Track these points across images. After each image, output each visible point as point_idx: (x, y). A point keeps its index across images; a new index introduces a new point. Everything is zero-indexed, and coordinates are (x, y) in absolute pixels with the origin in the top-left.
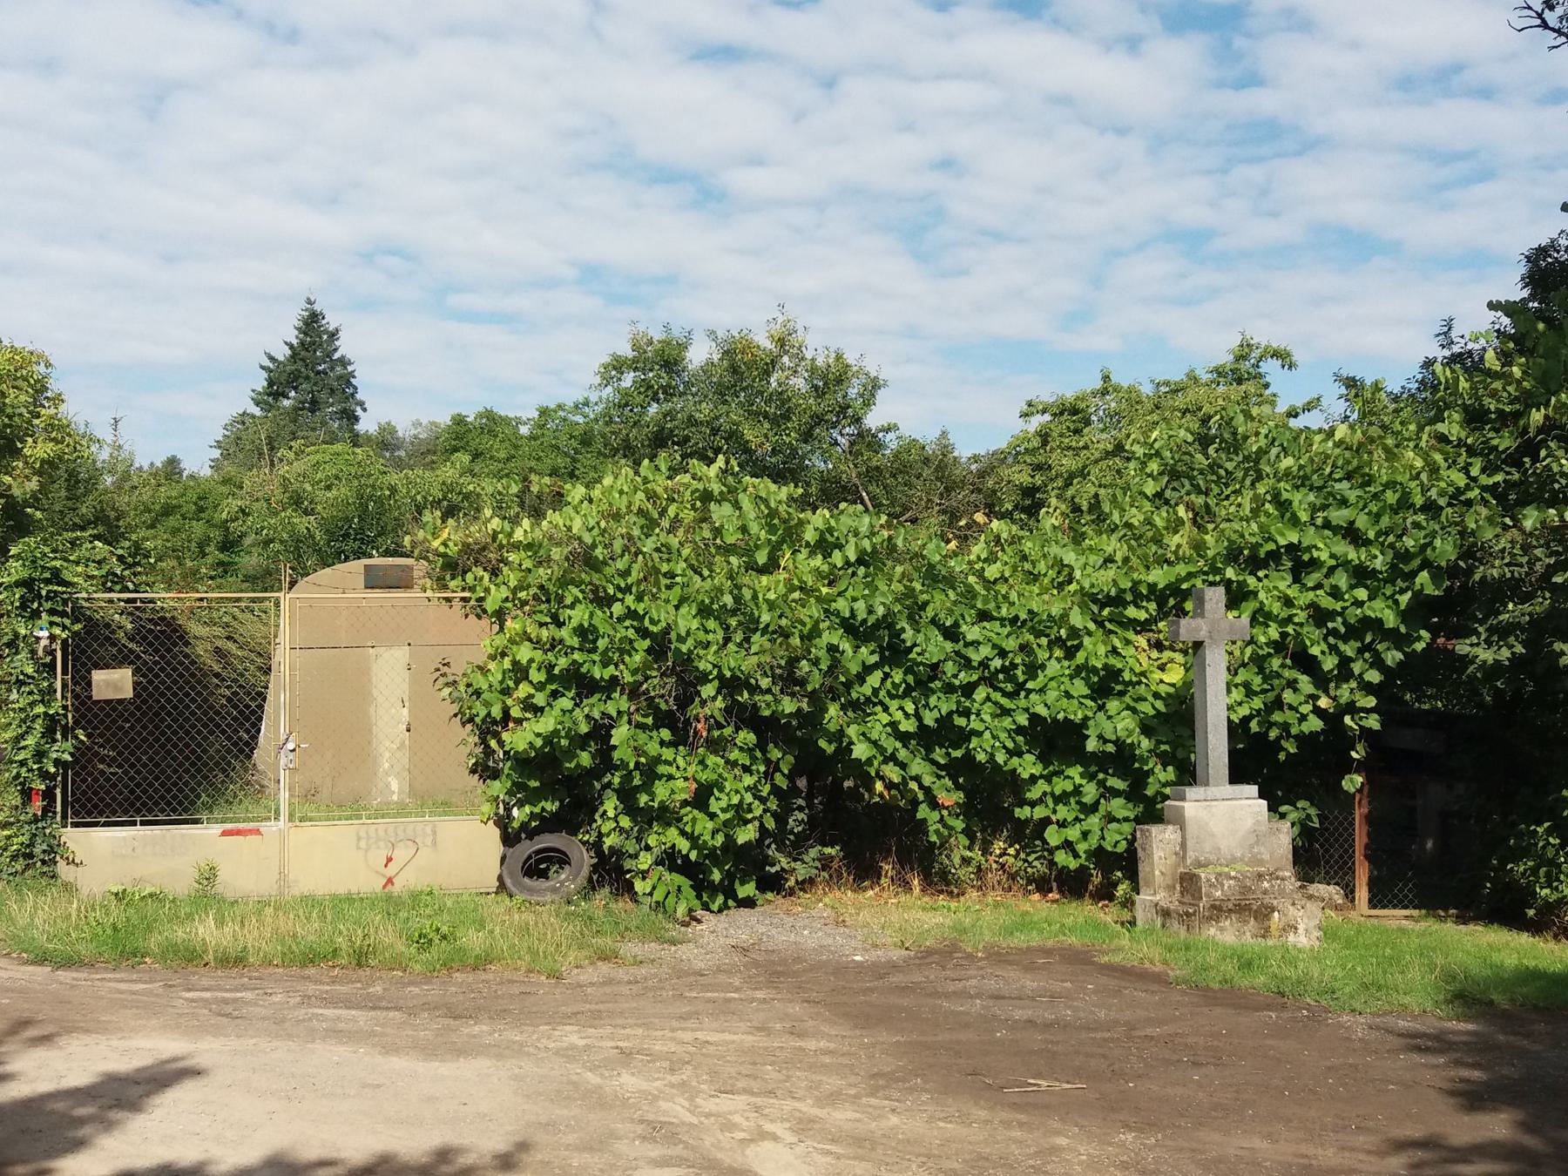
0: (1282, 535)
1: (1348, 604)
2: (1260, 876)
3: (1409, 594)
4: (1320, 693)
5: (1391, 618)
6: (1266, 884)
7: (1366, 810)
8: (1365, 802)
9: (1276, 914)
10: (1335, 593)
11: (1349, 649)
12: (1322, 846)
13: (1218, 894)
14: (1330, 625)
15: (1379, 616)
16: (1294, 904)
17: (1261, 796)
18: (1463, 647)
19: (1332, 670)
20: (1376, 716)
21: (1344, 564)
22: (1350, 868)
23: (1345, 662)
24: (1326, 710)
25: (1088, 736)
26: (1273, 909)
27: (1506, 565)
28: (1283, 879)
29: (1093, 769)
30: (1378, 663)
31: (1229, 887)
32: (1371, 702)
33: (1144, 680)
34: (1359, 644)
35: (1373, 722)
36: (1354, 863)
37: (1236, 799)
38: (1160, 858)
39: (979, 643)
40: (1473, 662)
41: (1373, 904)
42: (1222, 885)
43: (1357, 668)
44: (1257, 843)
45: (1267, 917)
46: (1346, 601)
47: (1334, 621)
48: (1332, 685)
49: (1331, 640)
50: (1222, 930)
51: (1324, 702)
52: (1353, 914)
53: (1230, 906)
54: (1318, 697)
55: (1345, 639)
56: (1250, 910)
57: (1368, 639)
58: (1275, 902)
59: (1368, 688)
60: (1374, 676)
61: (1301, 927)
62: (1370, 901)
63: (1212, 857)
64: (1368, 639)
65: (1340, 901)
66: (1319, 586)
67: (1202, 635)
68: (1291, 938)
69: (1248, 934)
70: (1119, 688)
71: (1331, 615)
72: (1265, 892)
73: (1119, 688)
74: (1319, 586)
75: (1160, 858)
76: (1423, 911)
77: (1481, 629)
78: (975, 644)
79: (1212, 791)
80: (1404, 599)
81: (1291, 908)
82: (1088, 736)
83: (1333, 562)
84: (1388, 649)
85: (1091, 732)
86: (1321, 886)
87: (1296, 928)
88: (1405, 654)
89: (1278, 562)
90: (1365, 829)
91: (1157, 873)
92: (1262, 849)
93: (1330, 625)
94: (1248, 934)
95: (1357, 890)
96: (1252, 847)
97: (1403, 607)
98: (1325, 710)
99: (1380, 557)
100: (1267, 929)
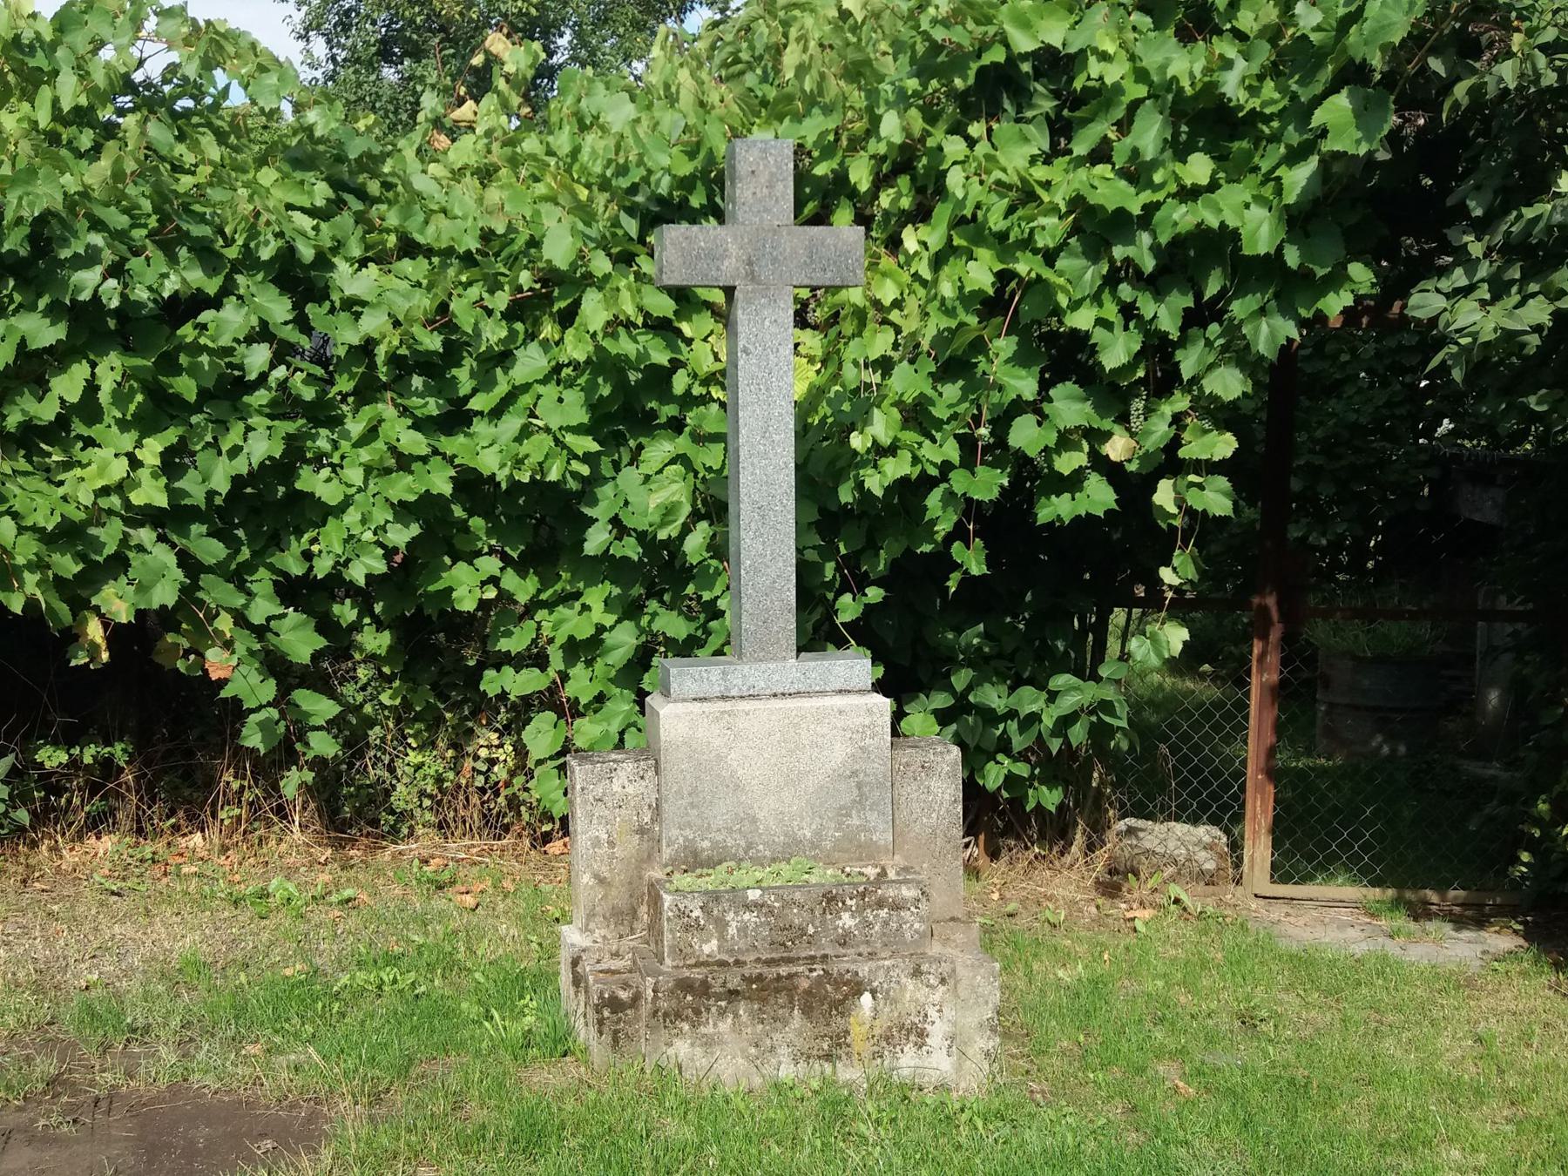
0: (1025, 24)
1: (1160, 196)
2: (831, 900)
3: (1311, 165)
4: (1107, 424)
5: (1265, 230)
6: (847, 920)
7: (1274, 678)
8: (1273, 659)
9: (866, 998)
10: (1137, 173)
11: (1166, 315)
12: (1174, 750)
13: (711, 947)
14: (1119, 252)
15: (1232, 223)
16: (917, 973)
17: (880, 687)
18: (1425, 302)
19: (1129, 368)
20: (1222, 482)
21: (1164, 92)
22: (1235, 797)
23: (1158, 350)
24: (1120, 465)
25: (592, 521)
26: (857, 988)
27: (1544, 48)
28: (897, 906)
29: (638, 590)
30: (1237, 352)
31: (743, 929)
32: (1224, 445)
33: (716, 393)
34: (1189, 301)
35: (1216, 499)
36: (1243, 788)
37: (808, 694)
38: (596, 843)
39: (364, 304)
40: (1443, 341)
41: (1280, 873)
42: (722, 925)
43: (1189, 362)
44: (860, 802)
45: (842, 1007)
46: (1156, 188)
47: (1130, 241)
48: (1138, 405)
49: (1126, 291)
50: (709, 1043)
51: (1117, 448)
52: (1231, 893)
53: (734, 982)
54: (1108, 435)
55: (1155, 284)
56: (791, 991)
57: (1212, 288)
58: (864, 970)
59: (1223, 415)
60: (1229, 384)
61: (937, 1033)
62: (1274, 867)
63: (735, 842)
64: (1212, 288)
65: (1210, 866)
66: (1101, 154)
67: (730, 268)
68: (907, 1061)
69: (783, 1051)
70: (669, 410)
71: (1121, 224)
72: (844, 941)
73: (669, 410)
74: (1101, 154)
75: (596, 843)
76: (1391, 892)
77: (1476, 249)
78: (354, 306)
79: (744, 673)
80: (1298, 178)
81: (910, 984)
82: (592, 521)
83: (1141, 91)
84: (1262, 311)
85: (600, 512)
86: (1180, 828)
87: (922, 1034)
88: (1302, 323)
89: (1023, 98)
90: (1270, 716)
91: (586, 879)
92: (872, 817)
93: (1119, 252)
94: (783, 1051)
95: (1248, 844)
96: (844, 812)
97: (1291, 198)
98: (1119, 466)
99: (1241, 65)
100: (840, 1040)
